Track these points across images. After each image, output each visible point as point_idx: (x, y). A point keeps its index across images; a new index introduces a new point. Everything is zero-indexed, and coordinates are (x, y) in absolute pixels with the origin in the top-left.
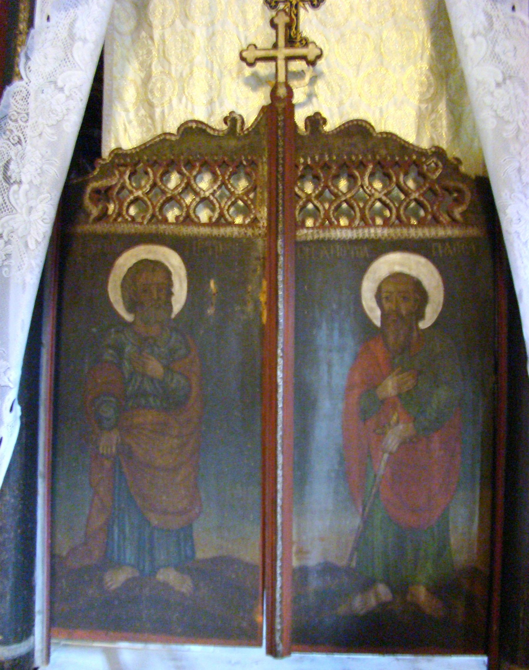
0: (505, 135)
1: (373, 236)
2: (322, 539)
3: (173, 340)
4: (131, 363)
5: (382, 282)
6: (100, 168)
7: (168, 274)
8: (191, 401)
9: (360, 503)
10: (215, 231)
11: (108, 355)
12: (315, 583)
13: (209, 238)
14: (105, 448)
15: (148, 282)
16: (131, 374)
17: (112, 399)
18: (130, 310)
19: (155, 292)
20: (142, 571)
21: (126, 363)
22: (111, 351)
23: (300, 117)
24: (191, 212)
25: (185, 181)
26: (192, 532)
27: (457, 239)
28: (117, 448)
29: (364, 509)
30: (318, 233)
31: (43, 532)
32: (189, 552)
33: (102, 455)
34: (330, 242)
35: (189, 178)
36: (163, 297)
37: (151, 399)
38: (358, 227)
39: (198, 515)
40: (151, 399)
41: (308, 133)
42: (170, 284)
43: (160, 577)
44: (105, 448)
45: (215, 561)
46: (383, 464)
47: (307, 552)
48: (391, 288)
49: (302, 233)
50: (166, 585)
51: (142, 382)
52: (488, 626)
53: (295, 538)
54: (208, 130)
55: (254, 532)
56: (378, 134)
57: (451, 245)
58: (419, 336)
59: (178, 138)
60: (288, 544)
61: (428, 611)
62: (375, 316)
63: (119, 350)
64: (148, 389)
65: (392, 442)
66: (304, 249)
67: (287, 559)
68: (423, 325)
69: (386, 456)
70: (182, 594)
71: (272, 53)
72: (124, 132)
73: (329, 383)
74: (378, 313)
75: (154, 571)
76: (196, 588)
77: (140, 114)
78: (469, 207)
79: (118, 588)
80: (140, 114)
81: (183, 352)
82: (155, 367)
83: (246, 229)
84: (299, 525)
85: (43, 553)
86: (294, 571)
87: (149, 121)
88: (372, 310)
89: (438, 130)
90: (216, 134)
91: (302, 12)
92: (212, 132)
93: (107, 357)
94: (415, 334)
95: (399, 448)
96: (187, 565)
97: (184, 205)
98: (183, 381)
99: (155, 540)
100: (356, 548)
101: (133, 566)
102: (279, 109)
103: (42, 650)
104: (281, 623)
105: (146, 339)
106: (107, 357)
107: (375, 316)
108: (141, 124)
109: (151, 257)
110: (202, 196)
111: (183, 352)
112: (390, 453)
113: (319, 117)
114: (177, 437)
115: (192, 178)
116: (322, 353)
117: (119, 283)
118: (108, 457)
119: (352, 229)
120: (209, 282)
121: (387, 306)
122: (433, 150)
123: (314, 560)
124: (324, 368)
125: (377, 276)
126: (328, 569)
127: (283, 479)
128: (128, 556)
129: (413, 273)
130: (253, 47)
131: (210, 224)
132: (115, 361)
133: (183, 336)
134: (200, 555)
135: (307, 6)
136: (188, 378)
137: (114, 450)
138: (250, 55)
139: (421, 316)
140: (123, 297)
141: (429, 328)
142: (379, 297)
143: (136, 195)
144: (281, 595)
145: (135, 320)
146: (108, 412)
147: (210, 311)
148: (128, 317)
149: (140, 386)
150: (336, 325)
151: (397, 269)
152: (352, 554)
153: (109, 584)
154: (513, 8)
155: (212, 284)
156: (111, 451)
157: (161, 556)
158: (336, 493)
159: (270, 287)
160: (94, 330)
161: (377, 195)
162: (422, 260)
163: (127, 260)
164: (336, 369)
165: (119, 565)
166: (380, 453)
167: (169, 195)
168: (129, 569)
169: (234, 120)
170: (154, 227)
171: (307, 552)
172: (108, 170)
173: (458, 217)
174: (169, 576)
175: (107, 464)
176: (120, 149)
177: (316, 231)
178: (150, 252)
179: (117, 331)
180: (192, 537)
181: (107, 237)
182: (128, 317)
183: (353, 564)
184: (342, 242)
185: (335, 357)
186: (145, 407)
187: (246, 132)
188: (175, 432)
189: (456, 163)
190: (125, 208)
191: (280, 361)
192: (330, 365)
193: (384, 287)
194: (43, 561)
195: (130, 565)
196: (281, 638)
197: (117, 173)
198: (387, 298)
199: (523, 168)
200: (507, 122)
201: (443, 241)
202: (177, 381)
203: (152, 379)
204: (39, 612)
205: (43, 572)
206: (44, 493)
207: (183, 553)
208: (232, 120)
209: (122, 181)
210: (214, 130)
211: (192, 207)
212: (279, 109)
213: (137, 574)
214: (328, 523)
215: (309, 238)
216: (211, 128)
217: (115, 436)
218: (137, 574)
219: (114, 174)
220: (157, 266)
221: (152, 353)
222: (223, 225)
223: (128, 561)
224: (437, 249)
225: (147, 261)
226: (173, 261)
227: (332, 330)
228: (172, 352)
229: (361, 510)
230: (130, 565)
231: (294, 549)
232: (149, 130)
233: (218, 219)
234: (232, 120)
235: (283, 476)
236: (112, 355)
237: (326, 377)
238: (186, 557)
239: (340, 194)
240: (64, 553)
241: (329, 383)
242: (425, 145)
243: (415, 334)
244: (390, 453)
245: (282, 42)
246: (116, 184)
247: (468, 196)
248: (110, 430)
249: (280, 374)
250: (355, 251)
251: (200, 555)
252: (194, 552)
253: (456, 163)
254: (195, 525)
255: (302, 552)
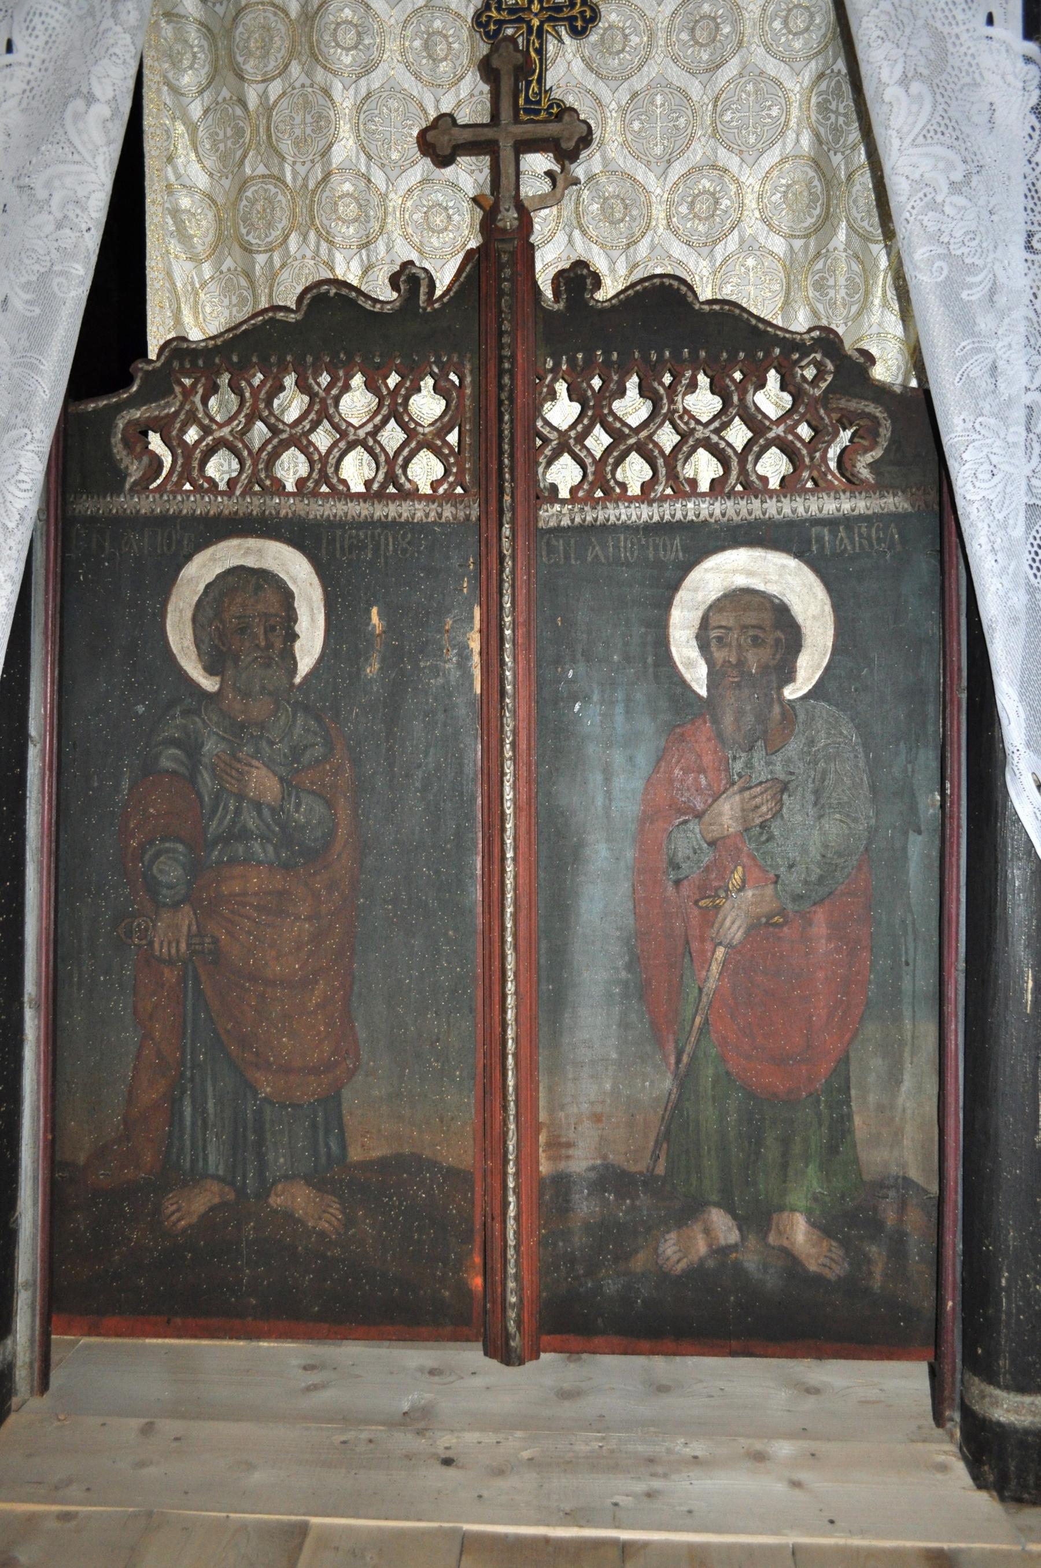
0: (964, 295)
1: (691, 516)
2: (597, 1118)
3: (298, 731)
4: (215, 776)
5: (711, 607)
6: (144, 382)
7: (287, 597)
8: (338, 847)
9: (671, 1047)
10: (380, 511)
11: (169, 759)
12: (585, 1207)
13: (369, 524)
14: (165, 944)
15: (247, 613)
16: (217, 798)
17: (180, 848)
18: (210, 670)
19: (260, 631)
20: (241, 1192)
21: (206, 776)
22: (173, 751)
23: (549, 260)
24: (330, 471)
25: (316, 407)
26: (339, 1105)
27: (862, 518)
28: (189, 945)
29: (678, 1061)
30: (582, 510)
31: (35, 1119)
32: (334, 1147)
33: (160, 960)
34: (606, 529)
35: (323, 401)
36: (279, 645)
37: (257, 847)
38: (664, 498)
39: (352, 1073)
40: (257, 847)
41: (561, 305)
42: (291, 617)
43: (276, 1201)
44: (165, 944)
45: (383, 1165)
46: (715, 968)
47: (569, 1145)
48: (726, 619)
49: (549, 515)
50: (288, 1216)
51: (238, 811)
52: (940, 1302)
53: (543, 1116)
54: (361, 301)
55: (462, 1103)
56: (703, 303)
57: (849, 528)
58: (784, 714)
59: (299, 316)
60: (529, 1128)
61: (813, 1267)
62: (697, 676)
63: (192, 749)
64: (251, 824)
65: (733, 923)
66: (554, 542)
67: (527, 1159)
68: (792, 692)
69: (720, 952)
70: (322, 1234)
71: (489, 134)
72: (187, 302)
73: (607, 809)
74: (703, 670)
75: (264, 1191)
76: (350, 1222)
77: (224, 268)
78: (887, 450)
79: (191, 1226)
80: (224, 268)
81: (318, 751)
82: (263, 782)
83: (441, 505)
84: (551, 1090)
85: (35, 1161)
86: (541, 1182)
87: (243, 282)
88: (690, 664)
89: (827, 294)
90: (378, 308)
91: (551, 46)
92: (368, 305)
93: (165, 763)
94: (777, 709)
95: (747, 934)
96: (330, 1176)
97: (316, 457)
98: (320, 808)
99: (268, 1126)
100: (666, 1136)
101: (221, 1180)
102: (502, 241)
103: (31, 1364)
104: (520, 1292)
105: (242, 726)
106: (165, 763)
107: (697, 676)
108: (227, 289)
109: (251, 562)
110: (351, 437)
111: (318, 751)
112: (729, 946)
113: (585, 271)
114: (308, 919)
115: (329, 401)
116: (592, 749)
117: (188, 614)
118: (170, 962)
119: (650, 504)
120: (368, 612)
121: (719, 655)
122: (816, 334)
123: (581, 1162)
124: (597, 778)
125: (700, 596)
126: (611, 1179)
127: (517, 1000)
128: (212, 1158)
129: (772, 589)
130: (449, 120)
131: (372, 494)
132: (182, 770)
133: (318, 719)
134: (355, 1154)
135: (563, 31)
136: (330, 804)
137: (183, 946)
138: (443, 142)
139: (789, 676)
140: (198, 643)
141: (804, 698)
142: (703, 641)
143: (218, 434)
144: (517, 1233)
145: (220, 689)
146: (171, 873)
147: (372, 669)
148: (209, 684)
149: (233, 822)
150: (620, 695)
151: (741, 581)
152: (657, 1144)
153: (174, 1218)
154: (990, 20)
155: (375, 619)
156: (178, 950)
157: (279, 1160)
158: (625, 1025)
159: (486, 620)
160: (141, 709)
161: (701, 433)
162: (792, 563)
163: (202, 569)
164: (619, 782)
165: (196, 1177)
166: (708, 946)
167: (284, 436)
168: (215, 1187)
169: (414, 281)
170: (257, 501)
171: (569, 1145)
172: (160, 384)
173: (865, 473)
174: (297, 1199)
175: (171, 976)
176: (184, 339)
177: (577, 507)
178: (248, 552)
179: (186, 713)
180: (340, 1118)
181: (162, 521)
182: (209, 684)
183: (661, 1169)
184: (628, 528)
185: (618, 757)
186: (246, 861)
187: (436, 306)
188: (304, 910)
189: (862, 360)
190: (195, 464)
191: (509, 768)
192: (608, 776)
193: (715, 620)
194: (35, 1178)
195: (216, 1177)
196: (519, 1323)
197: (178, 389)
198: (720, 639)
199: (1001, 364)
200: (972, 269)
201: (832, 523)
202: (306, 812)
203: (258, 806)
204: (26, 1285)
205: (35, 1204)
206: (38, 1039)
207: (323, 1150)
208: (408, 278)
209: (187, 407)
210: (376, 301)
211: (332, 461)
212: (502, 241)
213: (231, 1196)
214: (608, 1086)
215: (565, 522)
216: (367, 297)
217: (185, 918)
218: (231, 1196)
219: (171, 391)
220: (264, 580)
221: (257, 754)
222: (392, 497)
223: (211, 1170)
224: (820, 539)
225: (242, 568)
226: (295, 568)
227: (612, 703)
228: (296, 752)
229: (672, 1060)
230: (216, 1177)
231: (542, 1138)
232: (243, 301)
233: (384, 486)
234: (408, 278)
235: (516, 993)
236: (175, 759)
237: (599, 801)
238: (329, 1154)
239: (627, 431)
240: (82, 1158)
241: (607, 809)
242: (800, 322)
243: (777, 709)
244: (729, 946)
245: (506, 114)
246: (177, 413)
247: (885, 432)
248: (176, 905)
249: (508, 794)
250: (656, 548)
251: (355, 1154)
252: (344, 1148)
253: (862, 360)
254: (346, 1093)
255: (558, 1146)
